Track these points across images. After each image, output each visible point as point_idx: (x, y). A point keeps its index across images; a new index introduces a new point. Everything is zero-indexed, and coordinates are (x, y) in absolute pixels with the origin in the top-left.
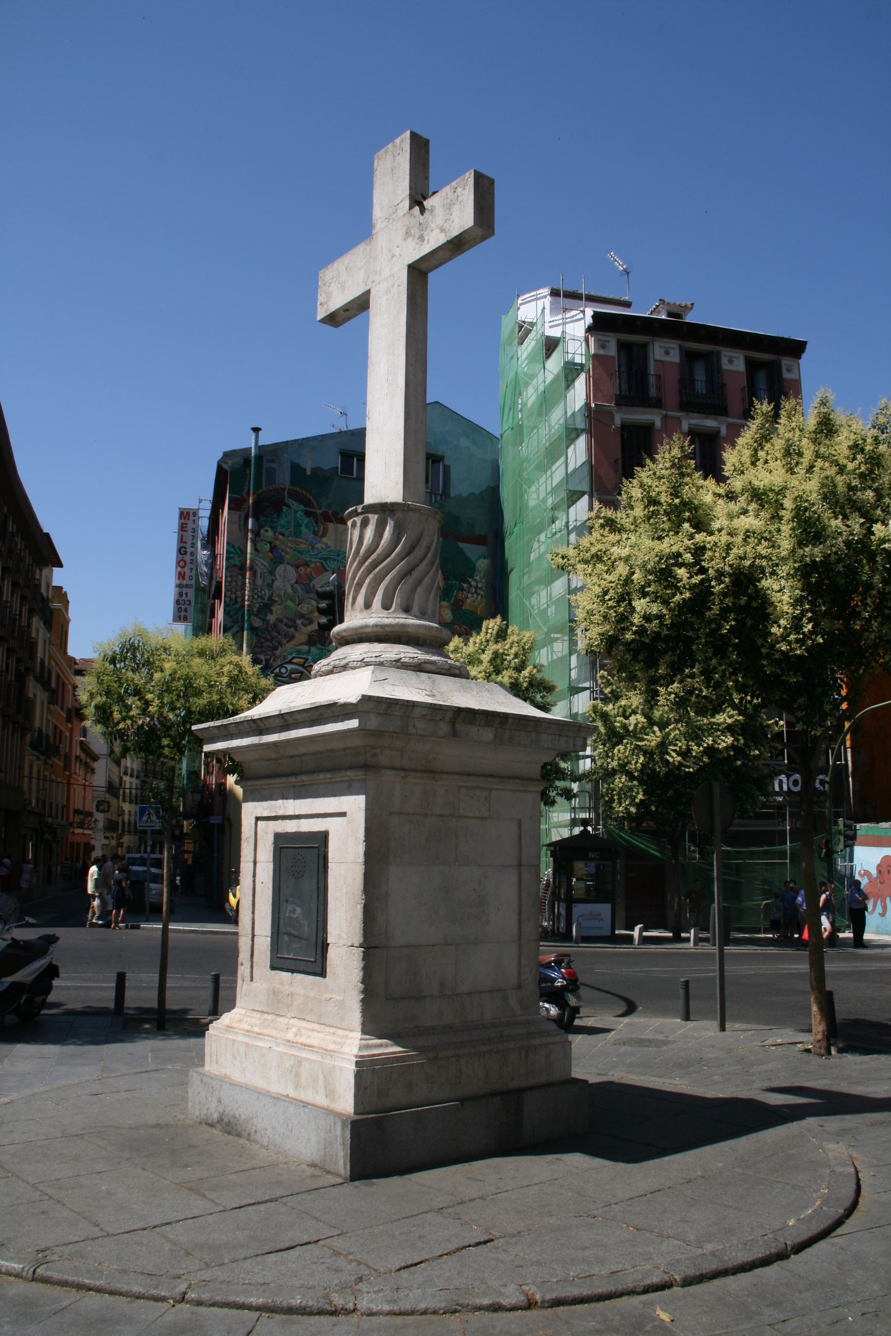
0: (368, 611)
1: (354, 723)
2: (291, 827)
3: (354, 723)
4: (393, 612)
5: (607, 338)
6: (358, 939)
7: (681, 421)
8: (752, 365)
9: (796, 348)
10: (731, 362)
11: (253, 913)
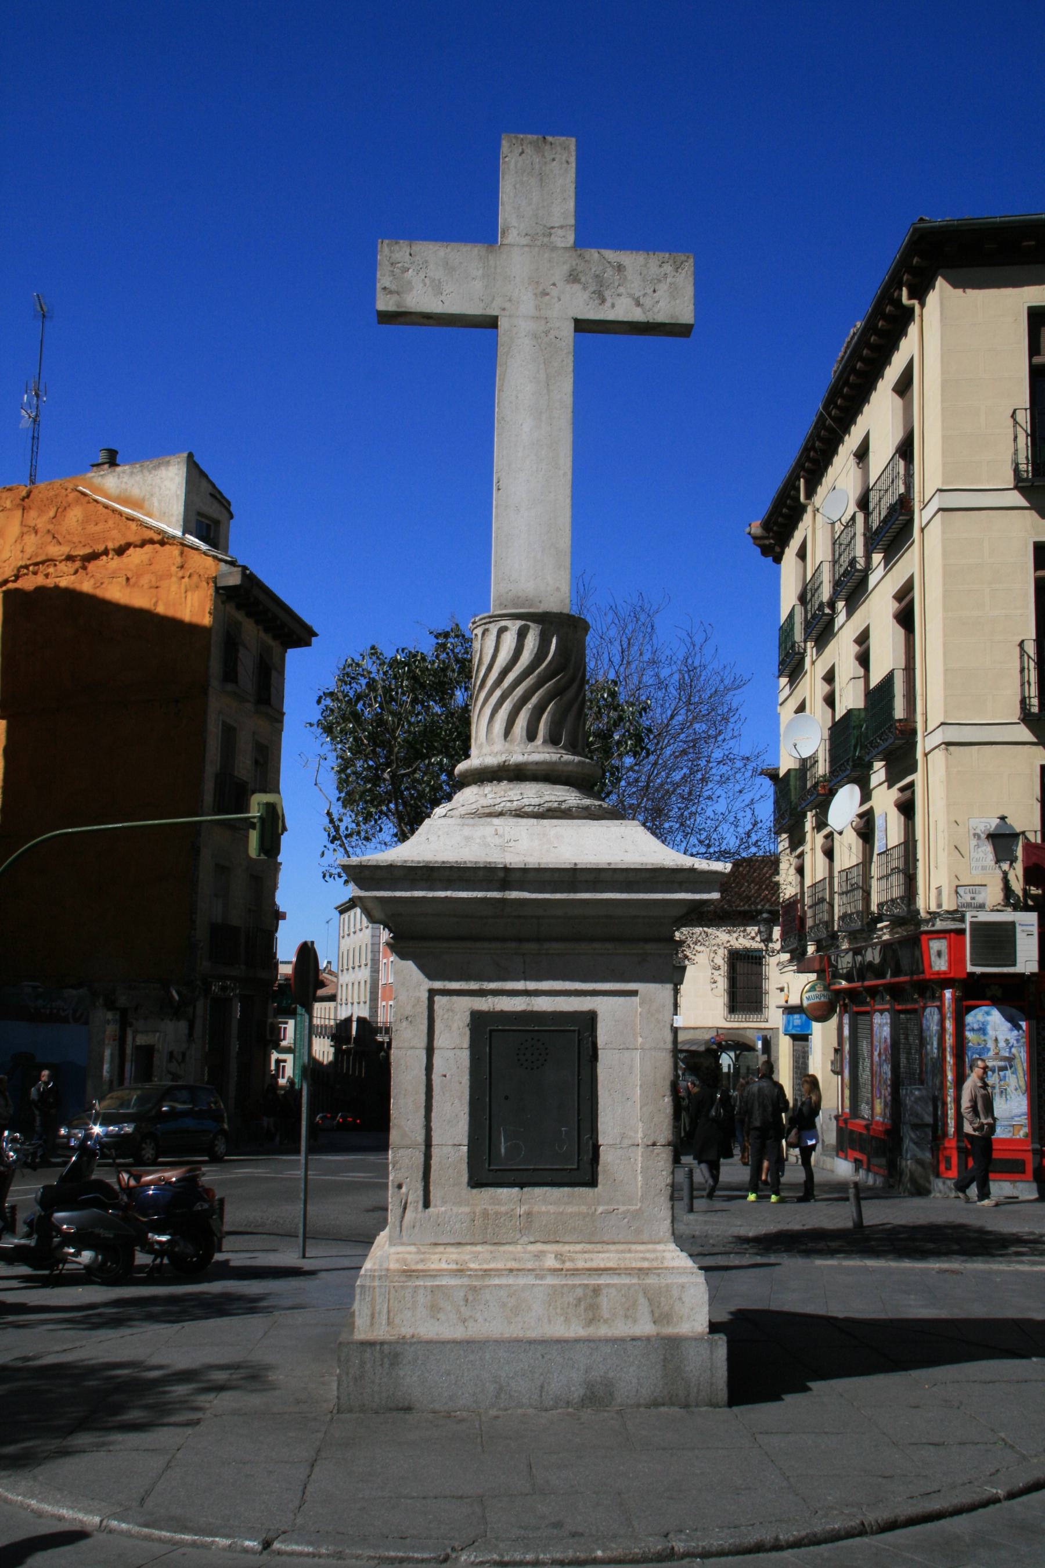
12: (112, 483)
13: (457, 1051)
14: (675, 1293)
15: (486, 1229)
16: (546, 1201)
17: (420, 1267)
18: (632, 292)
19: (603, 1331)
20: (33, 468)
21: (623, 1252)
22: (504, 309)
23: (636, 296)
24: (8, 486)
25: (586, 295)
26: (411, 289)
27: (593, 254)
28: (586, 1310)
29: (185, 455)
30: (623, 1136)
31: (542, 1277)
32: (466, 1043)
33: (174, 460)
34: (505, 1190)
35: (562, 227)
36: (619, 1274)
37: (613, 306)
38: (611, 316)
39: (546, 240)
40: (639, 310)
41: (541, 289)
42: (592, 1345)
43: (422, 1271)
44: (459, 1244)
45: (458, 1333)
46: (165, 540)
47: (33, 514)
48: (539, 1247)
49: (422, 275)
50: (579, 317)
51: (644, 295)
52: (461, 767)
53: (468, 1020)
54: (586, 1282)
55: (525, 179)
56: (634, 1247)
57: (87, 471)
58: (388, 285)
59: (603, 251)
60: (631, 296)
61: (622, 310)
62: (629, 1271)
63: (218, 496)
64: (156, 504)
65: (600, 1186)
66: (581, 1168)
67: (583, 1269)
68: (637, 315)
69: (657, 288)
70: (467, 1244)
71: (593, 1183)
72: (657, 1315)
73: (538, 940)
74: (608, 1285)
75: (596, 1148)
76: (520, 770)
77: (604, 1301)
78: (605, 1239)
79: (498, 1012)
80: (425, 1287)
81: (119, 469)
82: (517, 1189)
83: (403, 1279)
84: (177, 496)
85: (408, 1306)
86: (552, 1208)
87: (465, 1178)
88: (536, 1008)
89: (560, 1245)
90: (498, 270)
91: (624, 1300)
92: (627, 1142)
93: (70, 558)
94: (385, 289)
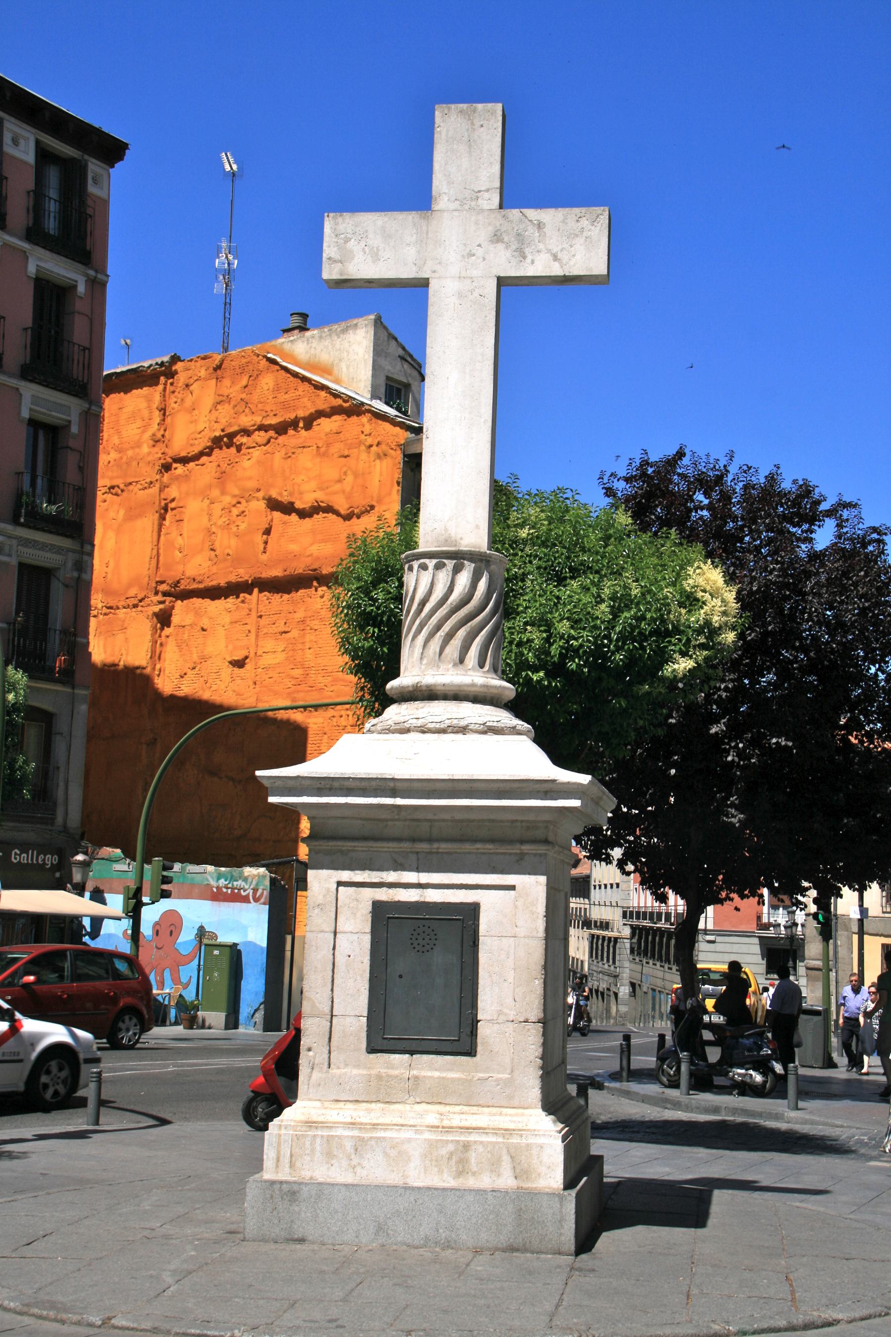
0: (461, 666)
1: (576, 803)
2: (383, 895)
3: (576, 803)
4: (488, 671)
5: (24, 133)
6: (535, 1012)
7: (27, 258)
8: (44, 155)
9: (112, 150)
10: (15, 142)
11: (332, 990)
12: (301, 348)
13: (362, 936)
14: (534, 1152)
15: (379, 1089)
16: (433, 1068)
17: (320, 1119)
18: (550, 247)
19: (471, 1182)
20: (226, 335)
21: (494, 1115)
22: (434, 272)
23: (555, 251)
24: (202, 355)
25: (508, 253)
26: (353, 258)
27: (515, 213)
28: (456, 1163)
29: (372, 317)
30: (500, 1013)
31: (421, 1132)
32: (368, 928)
33: (361, 321)
34: (397, 1056)
35: (487, 190)
36: (487, 1133)
37: (533, 262)
38: (531, 271)
39: (473, 203)
40: (557, 264)
41: (467, 250)
42: (458, 1193)
43: (322, 1123)
44: (357, 1101)
45: (349, 1179)
46: (355, 409)
47: (227, 382)
48: (424, 1106)
49: (363, 244)
50: (502, 275)
51: (561, 250)
52: (392, 685)
53: (370, 909)
54: (458, 1138)
55: (455, 147)
56: (505, 1110)
57: (278, 338)
58: (333, 255)
59: (525, 211)
60: (549, 251)
61: (539, 265)
62: (496, 1131)
63: (409, 360)
64: (344, 369)
65: (478, 1055)
66: (463, 1041)
67: (457, 1127)
68: (556, 270)
69: (573, 243)
70: (363, 1101)
71: (471, 1052)
72: (518, 1171)
73: (430, 840)
74: (475, 1142)
75: (475, 1022)
76: (431, 690)
77: (473, 1156)
78: (481, 1102)
79: (396, 902)
80: (322, 1136)
81: (308, 334)
82: (407, 1055)
83: (304, 1129)
84: (365, 360)
85: (307, 1152)
86: (436, 1074)
87: (364, 1045)
88: (428, 900)
89: (442, 1106)
90: (430, 235)
91: (489, 1156)
92: (502, 1018)
93: (262, 428)
94: (329, 259)
